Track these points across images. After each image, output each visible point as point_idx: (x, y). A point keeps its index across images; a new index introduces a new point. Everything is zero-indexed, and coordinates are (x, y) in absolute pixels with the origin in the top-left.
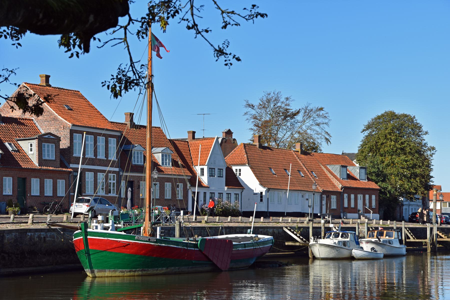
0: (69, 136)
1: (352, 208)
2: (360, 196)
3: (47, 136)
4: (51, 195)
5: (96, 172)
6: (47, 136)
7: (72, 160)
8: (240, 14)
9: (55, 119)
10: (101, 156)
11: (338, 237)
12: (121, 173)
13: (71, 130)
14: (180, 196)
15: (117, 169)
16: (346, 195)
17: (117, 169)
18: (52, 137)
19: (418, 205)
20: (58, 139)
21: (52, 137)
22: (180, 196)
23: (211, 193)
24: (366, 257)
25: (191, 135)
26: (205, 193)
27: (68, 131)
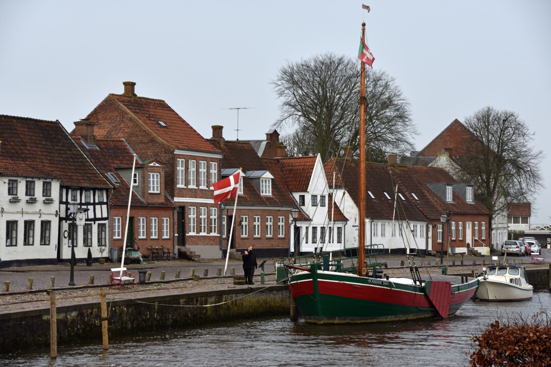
7: (176, 192)
26: (307, 228)
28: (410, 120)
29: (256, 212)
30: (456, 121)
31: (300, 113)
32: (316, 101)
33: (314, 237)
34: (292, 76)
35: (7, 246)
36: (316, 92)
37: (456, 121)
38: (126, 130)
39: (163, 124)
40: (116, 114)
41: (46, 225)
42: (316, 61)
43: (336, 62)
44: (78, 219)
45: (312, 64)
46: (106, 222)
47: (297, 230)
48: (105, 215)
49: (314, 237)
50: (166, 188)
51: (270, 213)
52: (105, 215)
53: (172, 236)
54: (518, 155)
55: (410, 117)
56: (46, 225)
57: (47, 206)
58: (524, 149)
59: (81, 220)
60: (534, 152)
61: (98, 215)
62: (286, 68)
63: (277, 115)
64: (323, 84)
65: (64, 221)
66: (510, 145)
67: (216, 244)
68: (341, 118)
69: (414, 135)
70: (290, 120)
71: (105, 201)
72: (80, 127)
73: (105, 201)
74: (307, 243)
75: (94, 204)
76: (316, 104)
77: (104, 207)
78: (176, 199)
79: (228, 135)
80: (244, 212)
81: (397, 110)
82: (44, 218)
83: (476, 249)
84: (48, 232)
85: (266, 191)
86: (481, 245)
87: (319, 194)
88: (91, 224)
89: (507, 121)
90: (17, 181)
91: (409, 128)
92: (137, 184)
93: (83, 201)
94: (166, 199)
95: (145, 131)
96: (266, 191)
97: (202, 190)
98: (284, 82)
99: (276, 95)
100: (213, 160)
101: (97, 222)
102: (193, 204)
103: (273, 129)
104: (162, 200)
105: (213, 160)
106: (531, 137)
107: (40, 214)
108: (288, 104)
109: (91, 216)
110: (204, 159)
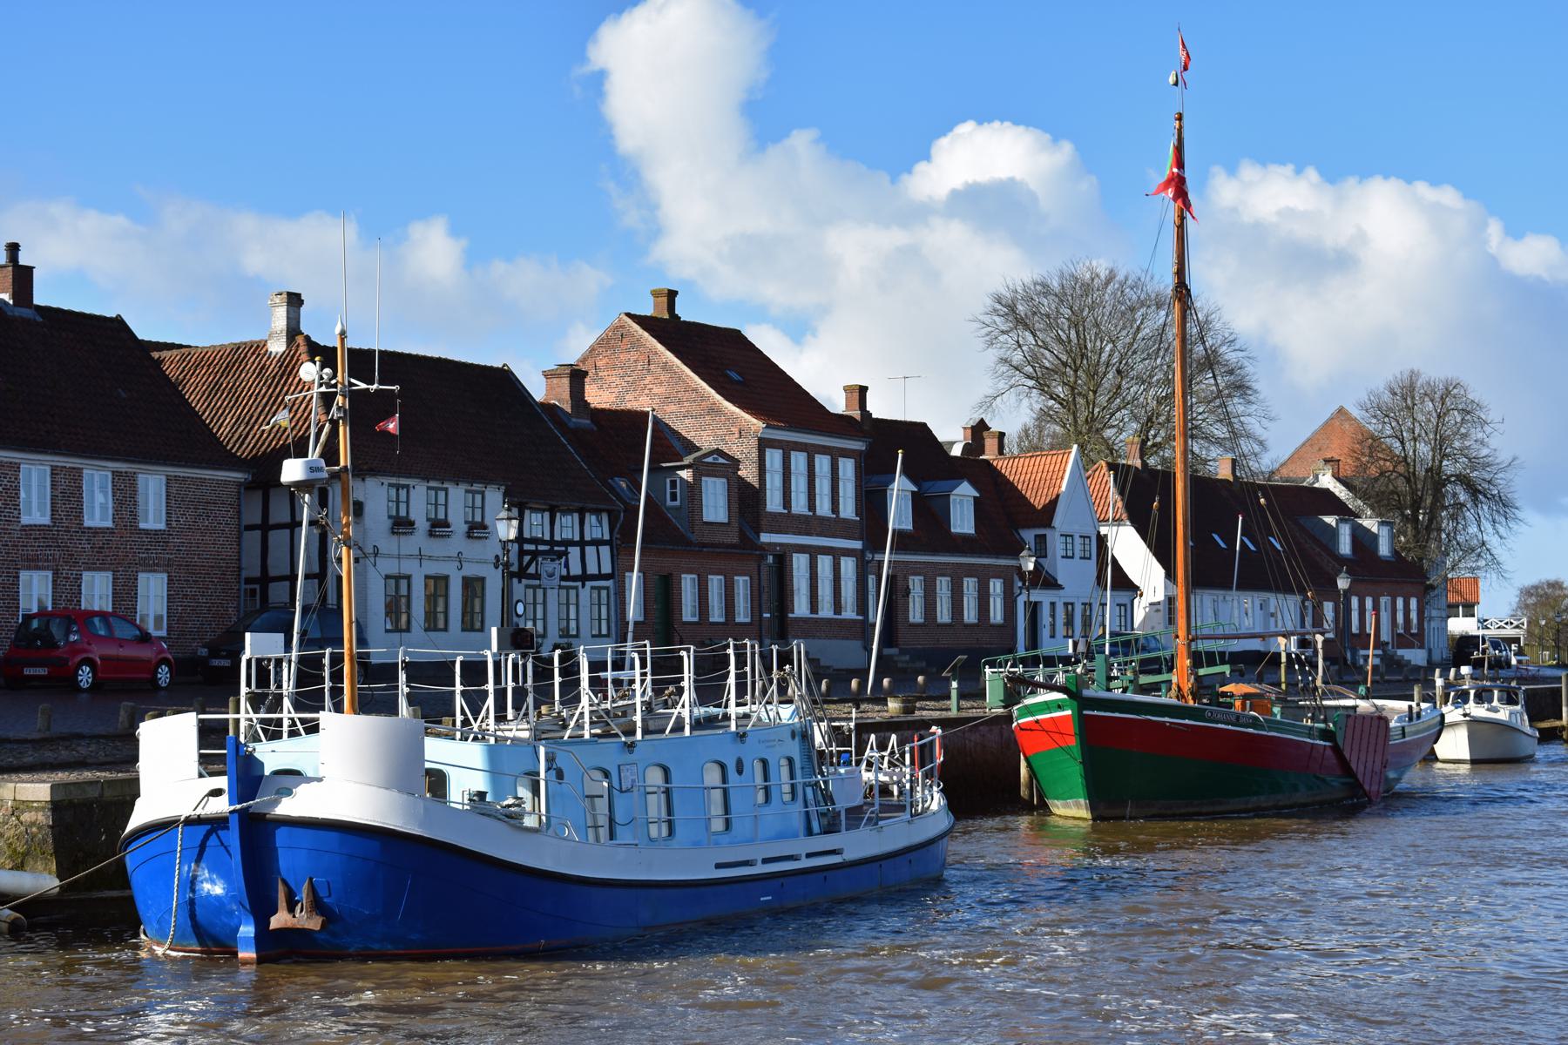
0: (755, 455)
1: (993, 626)
2: (799, 505)
3: (710, 460)
4: (722, 620)
5: (813, 552)
6: (710, 460)
7: (764, 522)
8: (1168, 168)
9: (714, 410)
10: (823, 508)
11: (1466, 701)
12: (869, 556)
13: (760, 440)
14: (997, 614)
15: (857, 545)
16: (1355, 601)
17: (857, 545)
18: (721, 460)
19: (673, 484)
20: (735, 463)
21: (721, 460)
22: (997, 614)
23: (1066, 604)
24: (1494, 757)
25: (856, 395)
26: (1053, 604)
27: (754, 442)
28: (1256, 392)
29: (941, 570)
30: (1341, 411)
31: (1031, 383)
32: (1064, 358)
33: (1069, 623)
34: (1012, 308)
35: (387, 631)
36: (1064, 337)
37: (1341, 411)
38: (655, 390)
39: (735, 376)
40: (633, 356)
41: (473, 587)
42: (1062, 276)
43: (1103, 276)
44: (544, 575)
45: (1055, 284)
46: (609, 583)
47: (1034, 609)
48: (607, 568)
49: (1069, 623)
50: (742, 513)
51: (971, 571)
52: (607, 568)
53: (757, 618)
54: (1474, 462)
55: (1255, 386)
56: (473, 587)
57: (477, 544)
58: (1485, 452)
59: (551, 575)
60: (1503, 457)
61: (592, 569)
62: (1004, 291)
63: (986, 386)
64: (1076, 323)
65: (515, 580)
66: (1457, 444)
67: (855, 638)
68: (1116, 394)
69: (1265, 422)
70: (1010, 397)
71: (607, 537)
72: (555, 381)
73: (607, 537)
74: (1053, 636)
75: (582, 544)
76: (1065, 364)
77: (605, 551)
78: (765, 538)
79: (879, 408)
80: (916, 569)
81: (1231, 372)
82: (471, 570)
83: (1400, 652)
84: (477, 602)
85: (963, 521)
86: (1410, 646)
87: (1076, 529)
88: (576, 588)
89: (1447, 397)
90: (407, 487)
91: (1254, 407)
92: (678, 503)
93: (557, 538)
94: (742, 534)
95: (695, 390)
96: (963, 521)
97: (823, 519)
98: (997, 319)
99: (980, 343)
100: (846, 453)
101: (589, 584)
102: (802, 549)
103: (976, 418)
104: (734, 538)
105: (846, 453)
106: (1497, 426)
107: (460, 559)
108: (1004, 361)
109: (576, 570)
110: (824, 450)
